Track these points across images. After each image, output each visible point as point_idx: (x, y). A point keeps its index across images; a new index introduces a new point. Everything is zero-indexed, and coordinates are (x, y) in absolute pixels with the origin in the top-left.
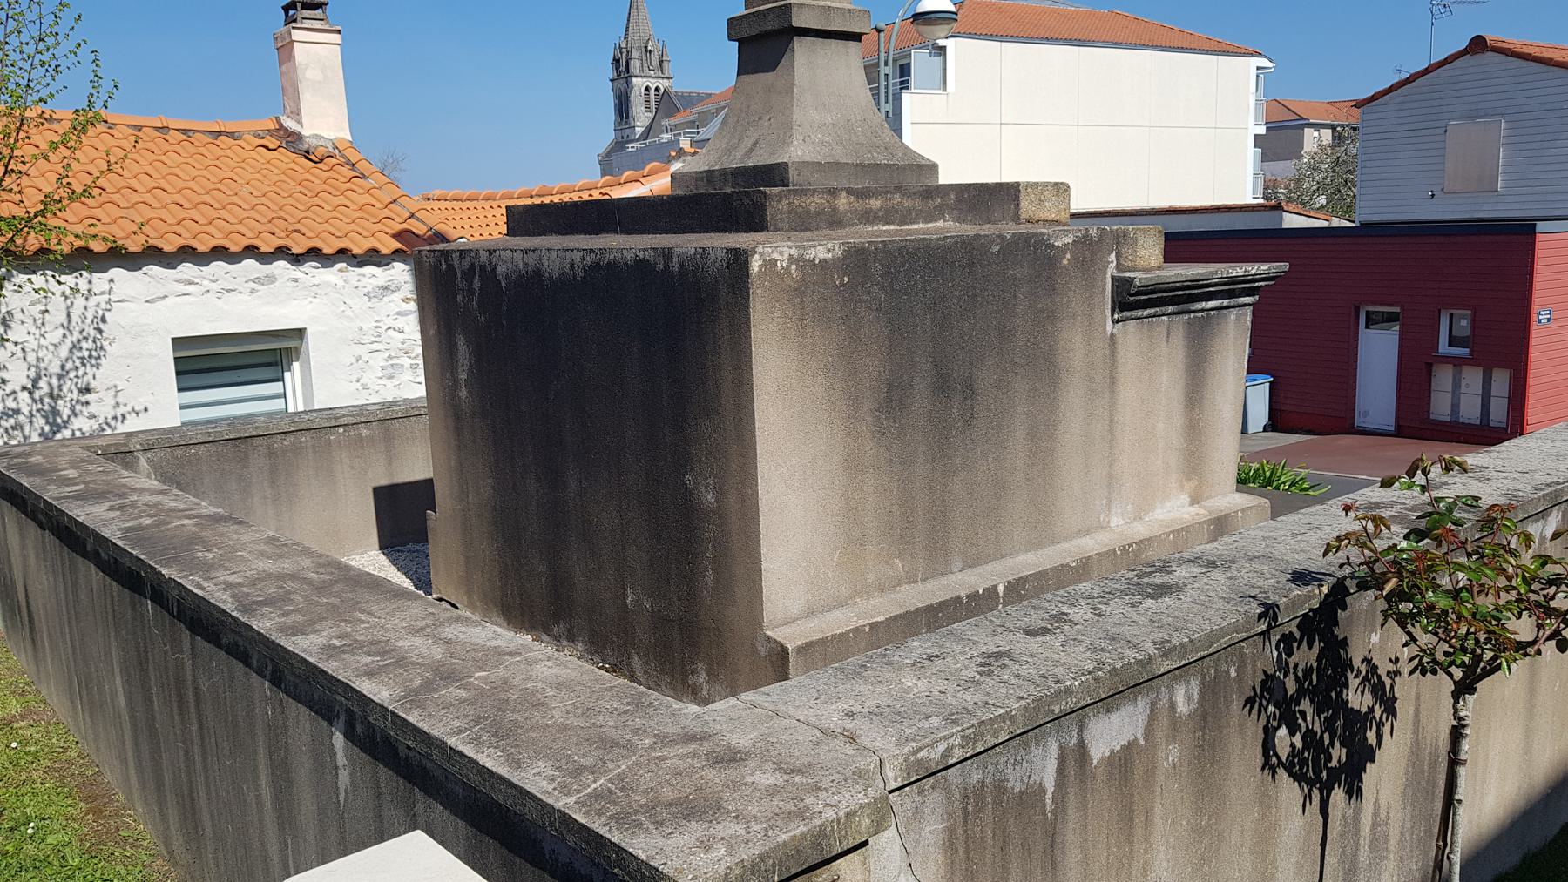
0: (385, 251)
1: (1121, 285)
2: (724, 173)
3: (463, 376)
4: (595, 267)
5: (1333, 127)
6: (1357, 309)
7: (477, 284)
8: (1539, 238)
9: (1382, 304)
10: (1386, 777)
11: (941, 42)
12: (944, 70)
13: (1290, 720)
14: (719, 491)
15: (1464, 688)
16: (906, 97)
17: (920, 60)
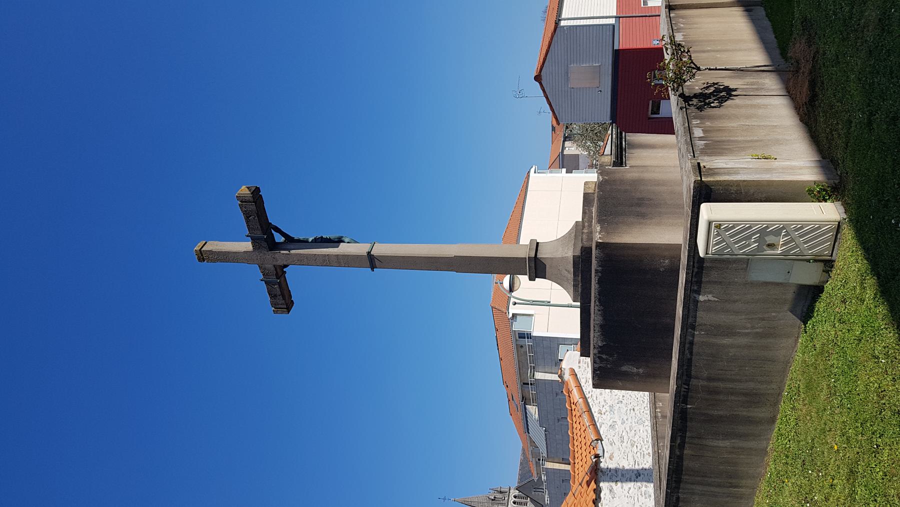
0: (595, 487)
1: (615, 164)
2: (574, 280)
3: (635, 370)
4: (600, 301)
5: (564, 141)
6: (650, 118)
7: (604, 356)
8: (621, 48)
9: (648, 108)
10: (732, 83)
11: (511, 315)
12: (523, 315)
13: (710, 103)
14: (664, 258)
15: (699, 69)
16: (534, 334)
17: (518, 326)
